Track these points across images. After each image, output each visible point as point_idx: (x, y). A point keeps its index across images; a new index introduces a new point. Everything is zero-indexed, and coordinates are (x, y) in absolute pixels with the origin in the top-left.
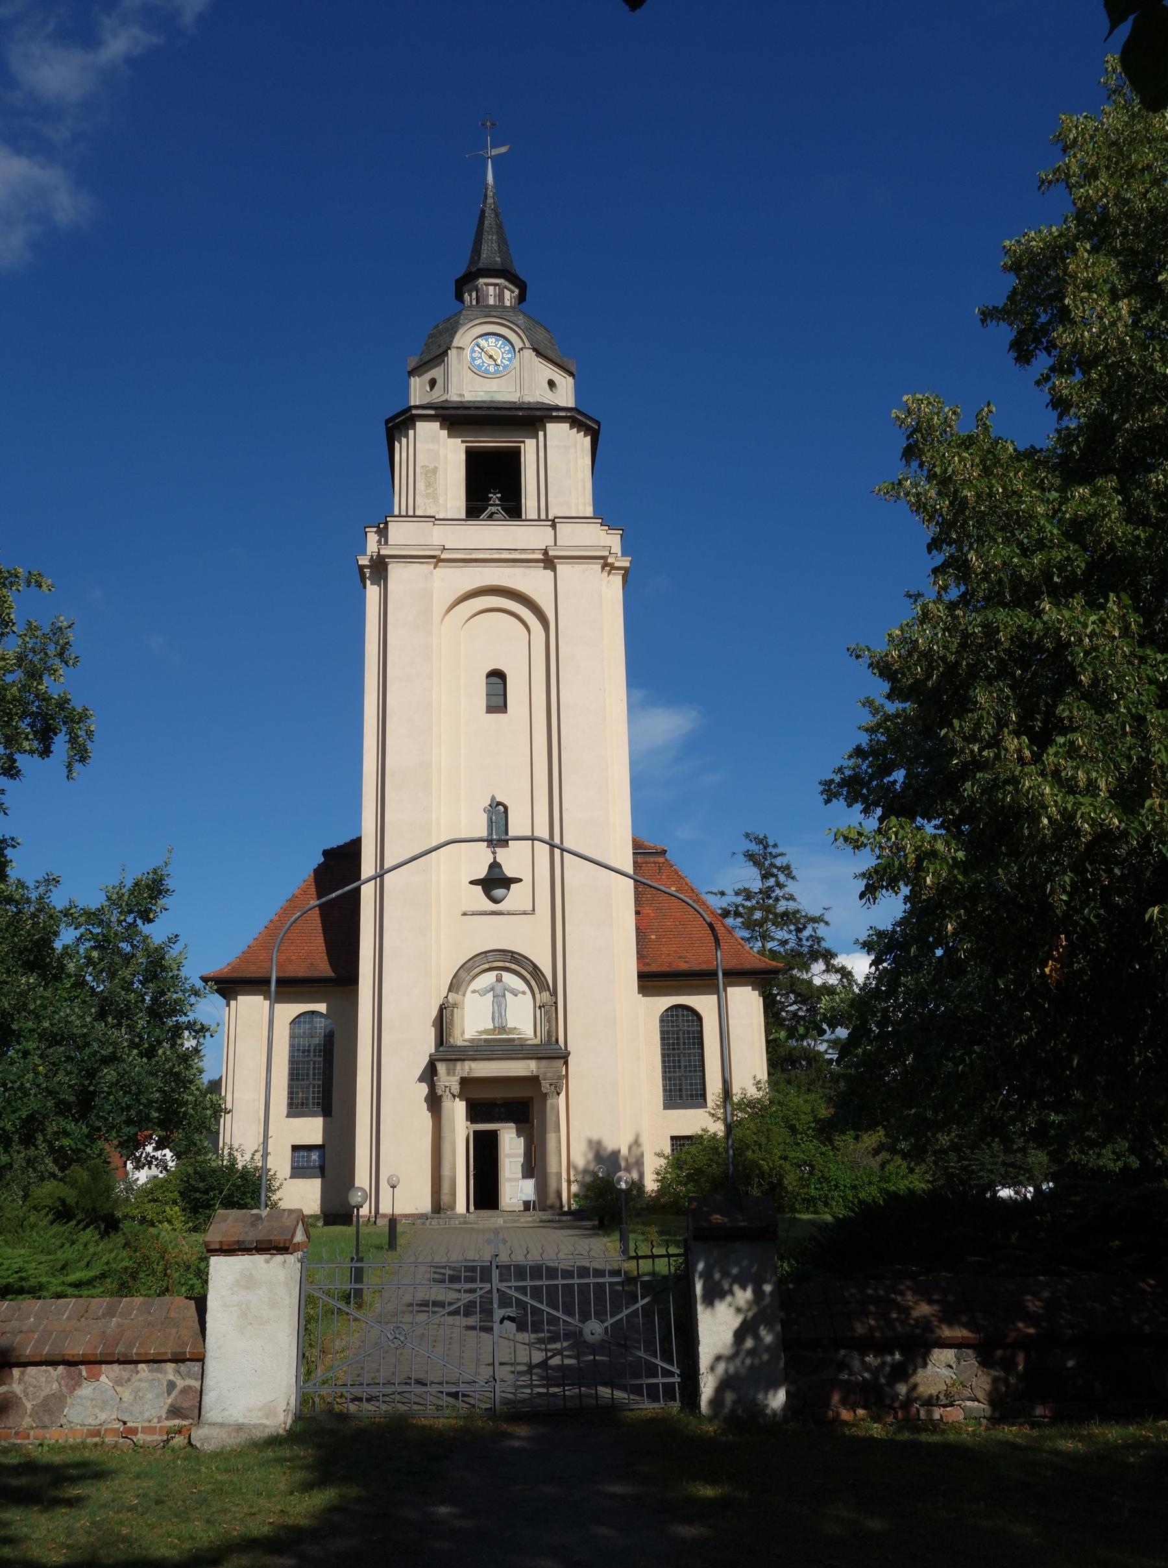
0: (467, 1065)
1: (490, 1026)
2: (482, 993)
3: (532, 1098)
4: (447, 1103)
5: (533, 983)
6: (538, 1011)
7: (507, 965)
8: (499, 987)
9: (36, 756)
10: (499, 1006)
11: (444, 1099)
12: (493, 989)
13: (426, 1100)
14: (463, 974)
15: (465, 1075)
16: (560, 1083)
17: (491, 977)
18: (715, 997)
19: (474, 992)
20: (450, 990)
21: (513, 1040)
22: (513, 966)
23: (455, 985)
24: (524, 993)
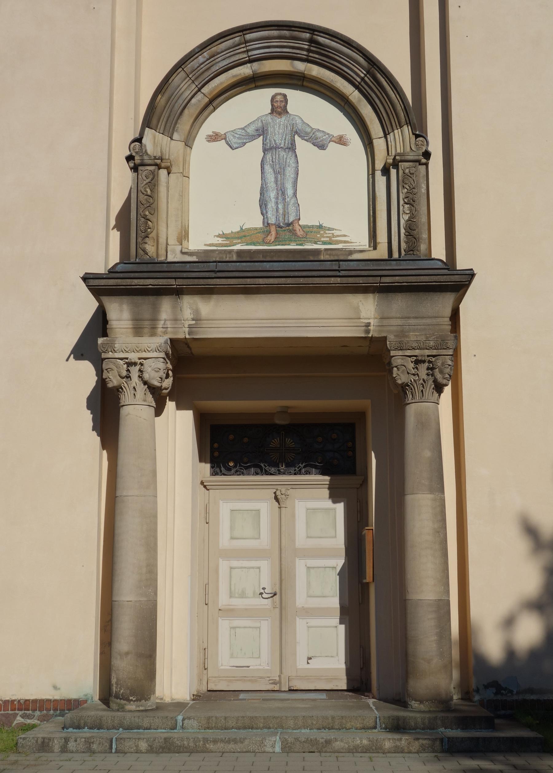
0: (190, 306)
1: (255, 221)
2: (235, 141)
3: (361, 415)
4: (135, 409)
5: (367, 111)
6: (381, 180)
7: (300, 66)
8: (278, 130)
9: (85, 375)
10: (279, 173)
11: (126, 398)
12: (262, 132)
13: (91, 403)
14: (184, 86)
15: (183, 333)
16: (443, 368)
17: (254, 104)
18: (345, 687)
19: (214, 138)
20: (147, 122)
21: (317, 252)
22: (315, 71)
23: (161, 112)
24: (341, 141)
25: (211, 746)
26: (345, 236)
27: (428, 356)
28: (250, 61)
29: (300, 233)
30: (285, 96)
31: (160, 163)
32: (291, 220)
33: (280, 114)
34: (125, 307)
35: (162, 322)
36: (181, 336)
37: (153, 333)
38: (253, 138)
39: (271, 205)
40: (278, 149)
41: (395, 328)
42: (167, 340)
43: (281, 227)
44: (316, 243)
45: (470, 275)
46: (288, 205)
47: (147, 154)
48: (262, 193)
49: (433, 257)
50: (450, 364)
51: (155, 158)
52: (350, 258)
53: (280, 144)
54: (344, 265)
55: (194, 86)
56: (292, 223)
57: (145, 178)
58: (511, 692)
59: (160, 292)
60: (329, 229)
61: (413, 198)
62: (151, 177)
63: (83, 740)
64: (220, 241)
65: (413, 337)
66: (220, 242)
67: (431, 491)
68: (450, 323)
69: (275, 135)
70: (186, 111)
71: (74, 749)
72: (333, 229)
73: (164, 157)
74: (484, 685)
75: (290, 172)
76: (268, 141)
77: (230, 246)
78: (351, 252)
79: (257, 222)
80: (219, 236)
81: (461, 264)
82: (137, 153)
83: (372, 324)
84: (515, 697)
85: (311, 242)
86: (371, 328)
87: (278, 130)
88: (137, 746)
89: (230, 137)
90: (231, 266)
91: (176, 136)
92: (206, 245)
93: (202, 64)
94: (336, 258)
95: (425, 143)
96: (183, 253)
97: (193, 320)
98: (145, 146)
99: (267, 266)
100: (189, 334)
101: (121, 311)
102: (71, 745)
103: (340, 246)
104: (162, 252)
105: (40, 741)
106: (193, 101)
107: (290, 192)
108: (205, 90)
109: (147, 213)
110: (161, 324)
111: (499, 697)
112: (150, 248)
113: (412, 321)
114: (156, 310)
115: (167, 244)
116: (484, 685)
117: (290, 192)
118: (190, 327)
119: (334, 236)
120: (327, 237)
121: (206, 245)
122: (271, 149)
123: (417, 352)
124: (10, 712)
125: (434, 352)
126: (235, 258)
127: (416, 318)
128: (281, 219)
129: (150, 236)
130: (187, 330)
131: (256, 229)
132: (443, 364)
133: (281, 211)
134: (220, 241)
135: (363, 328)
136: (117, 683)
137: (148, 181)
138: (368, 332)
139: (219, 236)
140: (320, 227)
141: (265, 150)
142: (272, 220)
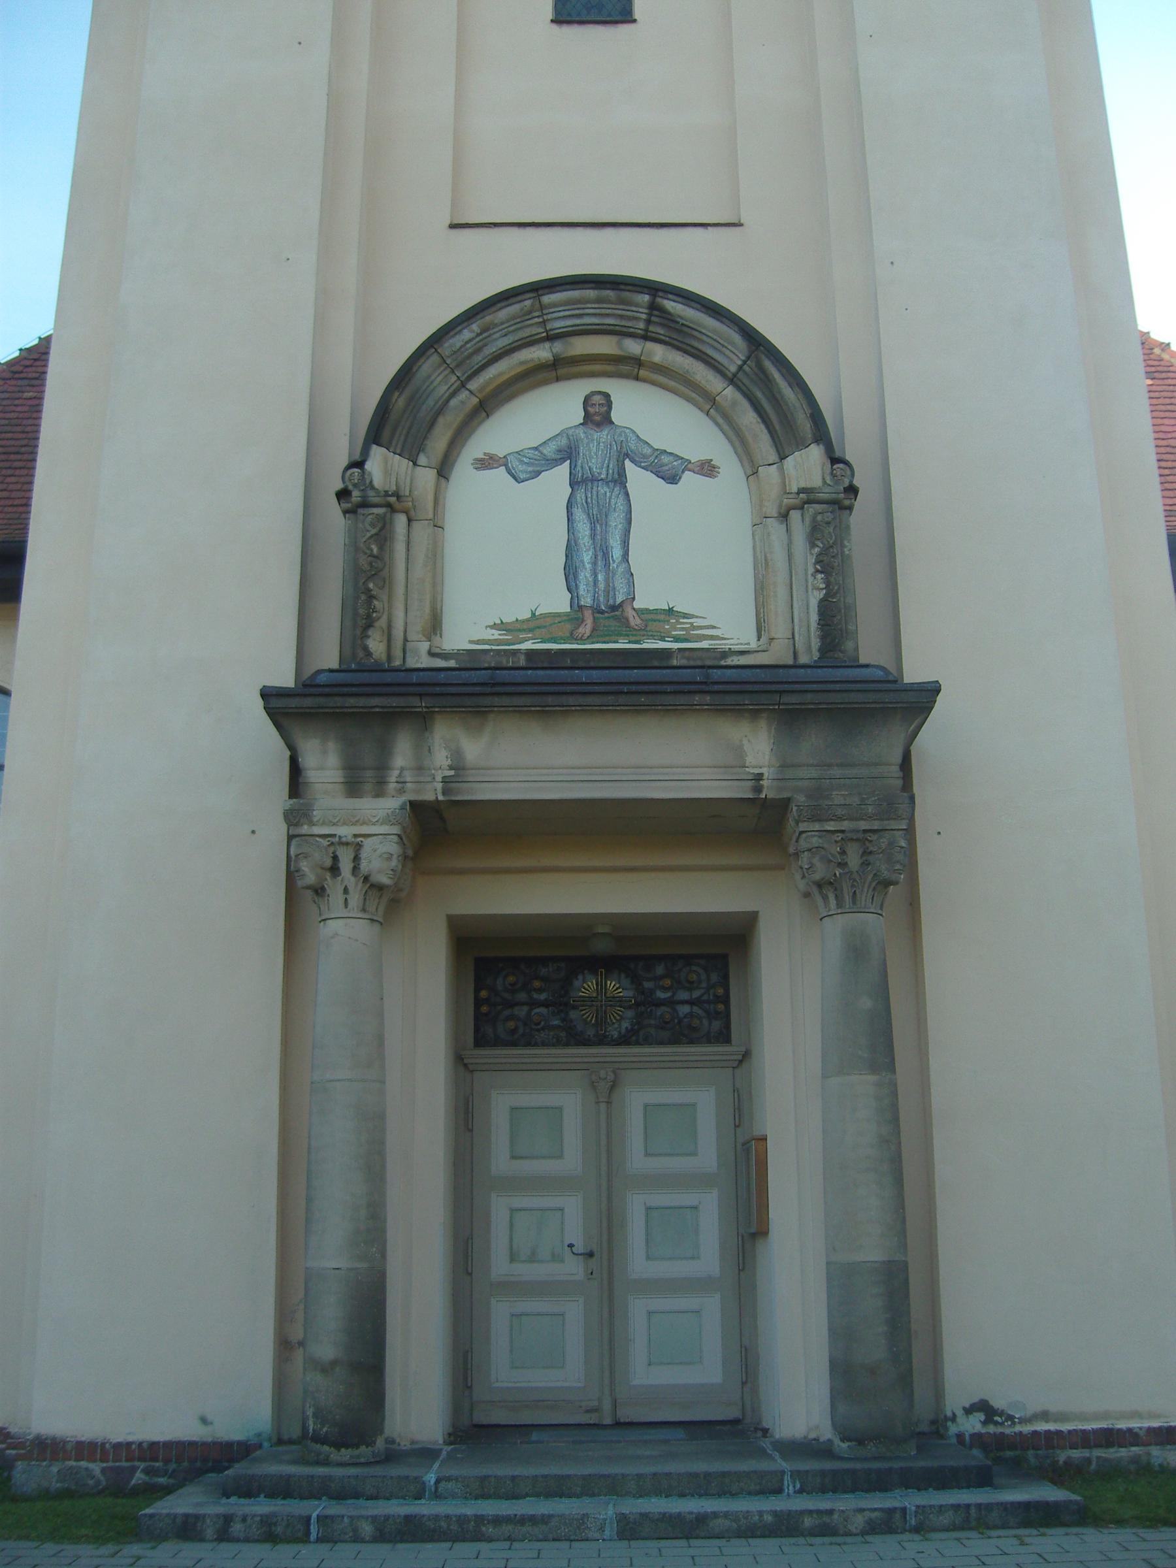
2: (529, 466)
7: (633, 347)
8: (596, 451)
10: (598, 521)
12: (569, 453)
15: (432, 792)
17: (552, 412)
21: (666, 654)
24: (707, 469)
25: (490, 1530)
26: (714, 627)
27: (865, 831)
28: (551, 338)
29: (635, 621)
30: (607, 396)
31: (395, 502)
32: (619, 601)
33: (599, 425)
34: (331, 745)
35: (396, 773)
36: (429, 796)
37: (380, 791)
38: (555, 462)
39: (585, 576)
40: (597, 478)
41: (806, 783)
42: (404, 803)
43: (602, 612)
44: (662, 639)
45: (932, 691)
46: (614, 574)
47: (372, 487)
48: (569, 555)
49: (862, 661)
50: (903, 845)
51: (387, 494)
52: (723, 663)
53: (600, 474)
54: (716, 674)
55: (454, 378)
56: (621, 605)
57: (368, 527)
58: (1011, 1418)
59: (391, 719)
60: (686, 616)
61: (831, 563)
62: (380, 525)
63: (258, 1519)
64: (496, 634)
65: (838, 798)
66: (496, 637)
67: (874, 1068)
68: (901, 774)
69: (591, 458)
70: (441, 420)
71: (242, 1535)
72: (692, 616)
73: (402, 493)
74: (964, 1408)
75: (616, 521)
76: (579, 468)
77: (514, 644)
78: (725, 654)
79: (561, 603)
80: (494, 626)
81: (914, 673)
82: (355, 485)
83: (766, 776)
84: (1018, 1428)
85: (653, 637)
86: (765, 783)
87: (596, 451)
88: (355, 1530)
89: (514, 463)
90: (519, 676)
91: (422, 460)
92: (471, 642)
93: (467, 343)
94: (699, 663)
95: (849, 472)
96: (431, 654)
97: (451, 768)
98: (370, 474)
99: (583, 675)
100: (444, 794)
101: (325, 752)
102: (237, 1528)
103: (705, 644)
104: (397, 653)
105: (179, 1521)
106: (454, 402)
107: (617, 553)
108: (473, 385)
109: (371, 585)
110: (393, 776)
111: (991, 1429)
112: (376, 645)
113: (836, 772)
114: (384, 752)
115: (406, 640)
116: (964, 1408)
117: (617, 553)
118: (445, 780)
119: (694, 628)
120: (683, 629)
121: (471, 642)
122: (584, 481)
123: (846, 825)
124: (125, 1464)
125: (876, 825)
126: (522, 662)
127: (841, 765)
128: (601, 599)
129: (377, 624)
130: (439, 786)
131: (558, 615)
132: (891, 844)
133: (602, 586)
134: (496, 634)
135: (750, 783)
136: (315, 1415)
137: (374, 531)
138: (758, 789)
139: (494, 626)
140: (670, 611)
141: (573, 484)
142: (587, 601)
